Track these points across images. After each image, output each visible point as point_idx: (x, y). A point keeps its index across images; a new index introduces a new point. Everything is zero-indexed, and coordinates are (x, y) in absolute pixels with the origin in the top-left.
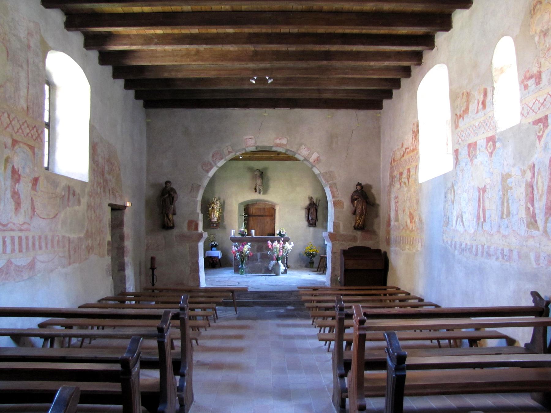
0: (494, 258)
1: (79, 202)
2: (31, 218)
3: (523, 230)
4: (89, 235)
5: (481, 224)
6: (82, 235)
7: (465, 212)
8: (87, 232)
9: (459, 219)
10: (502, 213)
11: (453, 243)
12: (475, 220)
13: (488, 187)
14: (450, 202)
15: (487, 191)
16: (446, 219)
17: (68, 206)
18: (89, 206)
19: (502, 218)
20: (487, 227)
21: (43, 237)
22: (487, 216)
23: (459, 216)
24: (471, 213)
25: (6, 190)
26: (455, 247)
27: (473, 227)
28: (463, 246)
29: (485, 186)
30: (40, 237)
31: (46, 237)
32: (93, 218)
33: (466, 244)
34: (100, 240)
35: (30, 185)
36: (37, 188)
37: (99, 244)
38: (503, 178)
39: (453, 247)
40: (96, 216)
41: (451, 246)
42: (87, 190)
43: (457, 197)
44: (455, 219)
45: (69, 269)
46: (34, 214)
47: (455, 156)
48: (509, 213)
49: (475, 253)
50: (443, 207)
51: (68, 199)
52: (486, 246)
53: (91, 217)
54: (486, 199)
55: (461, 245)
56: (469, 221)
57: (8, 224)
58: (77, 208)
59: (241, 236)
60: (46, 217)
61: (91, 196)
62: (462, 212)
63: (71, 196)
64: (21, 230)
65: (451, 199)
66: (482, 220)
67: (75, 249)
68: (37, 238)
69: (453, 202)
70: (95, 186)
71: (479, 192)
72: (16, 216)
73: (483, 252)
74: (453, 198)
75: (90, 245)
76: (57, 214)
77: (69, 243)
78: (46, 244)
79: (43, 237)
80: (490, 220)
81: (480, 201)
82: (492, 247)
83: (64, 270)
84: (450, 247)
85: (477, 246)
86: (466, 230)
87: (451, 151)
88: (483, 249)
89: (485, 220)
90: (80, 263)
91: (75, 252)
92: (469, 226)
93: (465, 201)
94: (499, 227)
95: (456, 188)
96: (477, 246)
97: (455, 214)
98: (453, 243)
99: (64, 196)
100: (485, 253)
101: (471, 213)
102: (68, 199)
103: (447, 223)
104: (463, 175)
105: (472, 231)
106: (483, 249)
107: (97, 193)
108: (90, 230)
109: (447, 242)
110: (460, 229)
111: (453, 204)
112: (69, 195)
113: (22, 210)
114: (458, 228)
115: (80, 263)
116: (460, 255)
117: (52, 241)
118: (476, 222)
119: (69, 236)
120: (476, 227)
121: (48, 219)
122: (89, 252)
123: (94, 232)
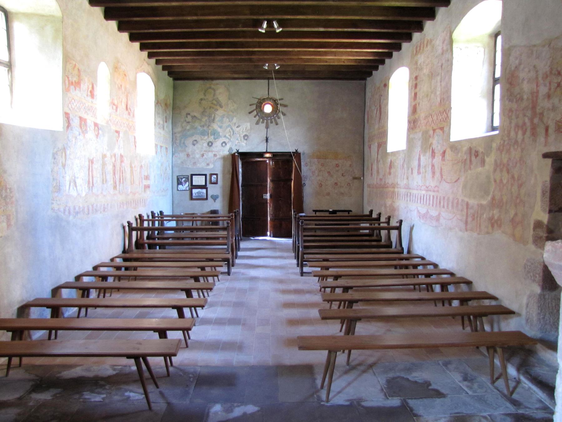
0: (99, 212)
1: (483, 162)
2: (440, 182)
3: (112, 192)
4: (495, 204)
5: (91, 188)
6: (484, 202)
7: (77, 178)
8: (493, 198)
9: (72, 184)
10: (103, 180)
11: (67, 209)
12: (87, 185)
13: (94, 160)
14: (60, 165)
15: (94, 162)
16: (57, 183)
17: (470, 169)
18: (498, 166)
19: (103, 183)
20: (95, 190)
21: (446, 198)
22: (95, 182)
23: (72, 181)
24: (83, 179)
25: (429, 165)
26: (69, 212)
27: (85, 191)
28: (77, 209)
29: (93, 159)
30: (444, 198)
31: (448, 198)
32: (505, 181)
33: (79, 207)
34: (516, 214)
35: (441, 157)
36: (445, 158)
37: (512, 221)
38: (103, 156)
39: (67, 213)
40: (513, 177)
41: (64, 212)
42: (494, 145)
43: (69, 162)
44: (68, 183)
45: (466, 234)
46: (442, 179)
47: (66, 119)
48: (106, 181)
49: (87, 213)
50: (50, 170)
51: (471, 161)
52: (95, 205)
53: (501, 181)
54: (94, 170)
55: (75, 209)
56: (81, 185)
57: (429, 186)
58: (480, 169)
59: (263, 184)
60: (449, 181)
61: (501, 151)
62: (75, 177)
63: (473, 158)
64: (434, 191)
65: (62, 162)
66: (91, 185)
67: (474, 216)
68: (442, 198)
69: (64, 166)
70: (512, 134)
71: (89, 162)
72: (433, 181)
73: (93, 210)
74: (64, 162)
75: (496, 217)
76: (459, 179)
77: (467, 208)
78: (448, 204)
79: (446, 198)
80: (96, 185)
81: (90, 169)
82: (99, 205)
83: (460, 233)
84: (62, 214)
85: (88, 206)
86: (79, 194)
87: (154, 145)
88: (93, 207)
89: (93, 184)
90: (479, 234)
91: (473, 219)
92: (82, 190)
93: (78, 167)
94: (102, 190)
95: (68, 152)
96: (88, 206)
97: (68, 178)
98: (67, 209)
99: (466, 160)
100: (94, 210)
101: (83, 179)
102: (471, 161)
103: (58, 189)
104: (75, 142)
105: (84, 194)
106: (93, 207)
107: (516, 142)
108: (497, 197)
109: (59, 209)
110: (74, 193)
111: (64, 169)
112: (471, 157)
113: (436, 177)
114: (71, 193)
115: (479, 234)
116: (74, 218)
117: (453, 203)
118: (88, 187)
119: (468, 200)
120: (88, 191)
121: (451, 183)
122: (493, 226)
123: (505, 200)
